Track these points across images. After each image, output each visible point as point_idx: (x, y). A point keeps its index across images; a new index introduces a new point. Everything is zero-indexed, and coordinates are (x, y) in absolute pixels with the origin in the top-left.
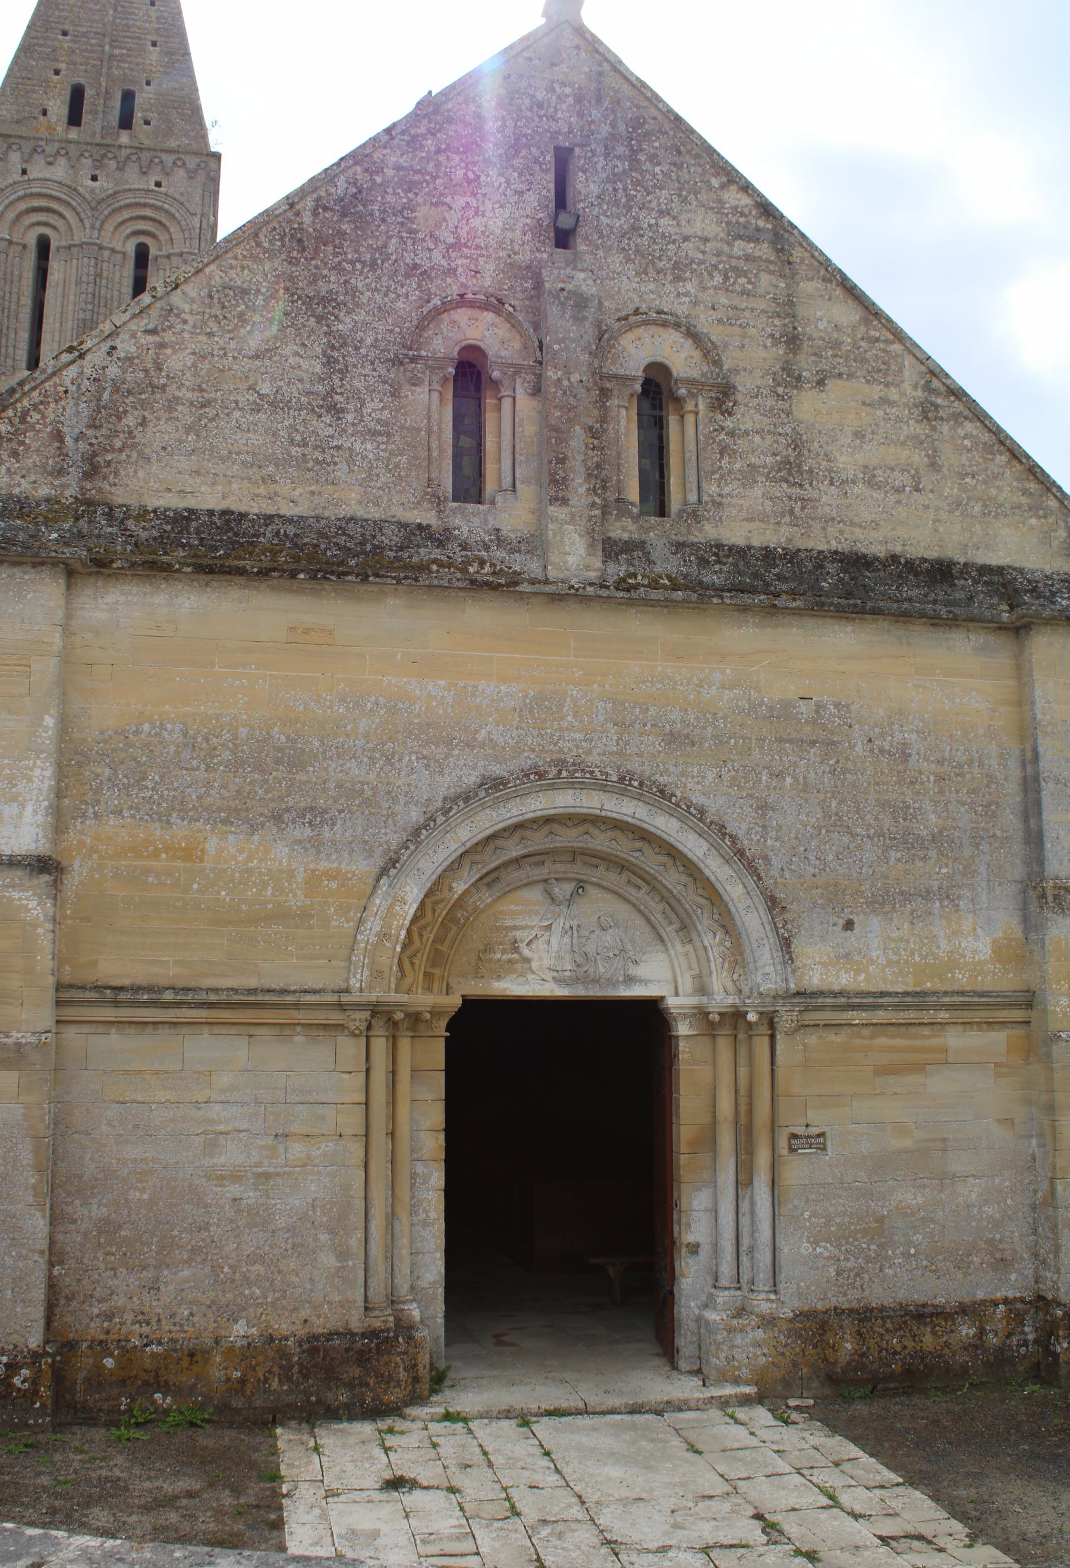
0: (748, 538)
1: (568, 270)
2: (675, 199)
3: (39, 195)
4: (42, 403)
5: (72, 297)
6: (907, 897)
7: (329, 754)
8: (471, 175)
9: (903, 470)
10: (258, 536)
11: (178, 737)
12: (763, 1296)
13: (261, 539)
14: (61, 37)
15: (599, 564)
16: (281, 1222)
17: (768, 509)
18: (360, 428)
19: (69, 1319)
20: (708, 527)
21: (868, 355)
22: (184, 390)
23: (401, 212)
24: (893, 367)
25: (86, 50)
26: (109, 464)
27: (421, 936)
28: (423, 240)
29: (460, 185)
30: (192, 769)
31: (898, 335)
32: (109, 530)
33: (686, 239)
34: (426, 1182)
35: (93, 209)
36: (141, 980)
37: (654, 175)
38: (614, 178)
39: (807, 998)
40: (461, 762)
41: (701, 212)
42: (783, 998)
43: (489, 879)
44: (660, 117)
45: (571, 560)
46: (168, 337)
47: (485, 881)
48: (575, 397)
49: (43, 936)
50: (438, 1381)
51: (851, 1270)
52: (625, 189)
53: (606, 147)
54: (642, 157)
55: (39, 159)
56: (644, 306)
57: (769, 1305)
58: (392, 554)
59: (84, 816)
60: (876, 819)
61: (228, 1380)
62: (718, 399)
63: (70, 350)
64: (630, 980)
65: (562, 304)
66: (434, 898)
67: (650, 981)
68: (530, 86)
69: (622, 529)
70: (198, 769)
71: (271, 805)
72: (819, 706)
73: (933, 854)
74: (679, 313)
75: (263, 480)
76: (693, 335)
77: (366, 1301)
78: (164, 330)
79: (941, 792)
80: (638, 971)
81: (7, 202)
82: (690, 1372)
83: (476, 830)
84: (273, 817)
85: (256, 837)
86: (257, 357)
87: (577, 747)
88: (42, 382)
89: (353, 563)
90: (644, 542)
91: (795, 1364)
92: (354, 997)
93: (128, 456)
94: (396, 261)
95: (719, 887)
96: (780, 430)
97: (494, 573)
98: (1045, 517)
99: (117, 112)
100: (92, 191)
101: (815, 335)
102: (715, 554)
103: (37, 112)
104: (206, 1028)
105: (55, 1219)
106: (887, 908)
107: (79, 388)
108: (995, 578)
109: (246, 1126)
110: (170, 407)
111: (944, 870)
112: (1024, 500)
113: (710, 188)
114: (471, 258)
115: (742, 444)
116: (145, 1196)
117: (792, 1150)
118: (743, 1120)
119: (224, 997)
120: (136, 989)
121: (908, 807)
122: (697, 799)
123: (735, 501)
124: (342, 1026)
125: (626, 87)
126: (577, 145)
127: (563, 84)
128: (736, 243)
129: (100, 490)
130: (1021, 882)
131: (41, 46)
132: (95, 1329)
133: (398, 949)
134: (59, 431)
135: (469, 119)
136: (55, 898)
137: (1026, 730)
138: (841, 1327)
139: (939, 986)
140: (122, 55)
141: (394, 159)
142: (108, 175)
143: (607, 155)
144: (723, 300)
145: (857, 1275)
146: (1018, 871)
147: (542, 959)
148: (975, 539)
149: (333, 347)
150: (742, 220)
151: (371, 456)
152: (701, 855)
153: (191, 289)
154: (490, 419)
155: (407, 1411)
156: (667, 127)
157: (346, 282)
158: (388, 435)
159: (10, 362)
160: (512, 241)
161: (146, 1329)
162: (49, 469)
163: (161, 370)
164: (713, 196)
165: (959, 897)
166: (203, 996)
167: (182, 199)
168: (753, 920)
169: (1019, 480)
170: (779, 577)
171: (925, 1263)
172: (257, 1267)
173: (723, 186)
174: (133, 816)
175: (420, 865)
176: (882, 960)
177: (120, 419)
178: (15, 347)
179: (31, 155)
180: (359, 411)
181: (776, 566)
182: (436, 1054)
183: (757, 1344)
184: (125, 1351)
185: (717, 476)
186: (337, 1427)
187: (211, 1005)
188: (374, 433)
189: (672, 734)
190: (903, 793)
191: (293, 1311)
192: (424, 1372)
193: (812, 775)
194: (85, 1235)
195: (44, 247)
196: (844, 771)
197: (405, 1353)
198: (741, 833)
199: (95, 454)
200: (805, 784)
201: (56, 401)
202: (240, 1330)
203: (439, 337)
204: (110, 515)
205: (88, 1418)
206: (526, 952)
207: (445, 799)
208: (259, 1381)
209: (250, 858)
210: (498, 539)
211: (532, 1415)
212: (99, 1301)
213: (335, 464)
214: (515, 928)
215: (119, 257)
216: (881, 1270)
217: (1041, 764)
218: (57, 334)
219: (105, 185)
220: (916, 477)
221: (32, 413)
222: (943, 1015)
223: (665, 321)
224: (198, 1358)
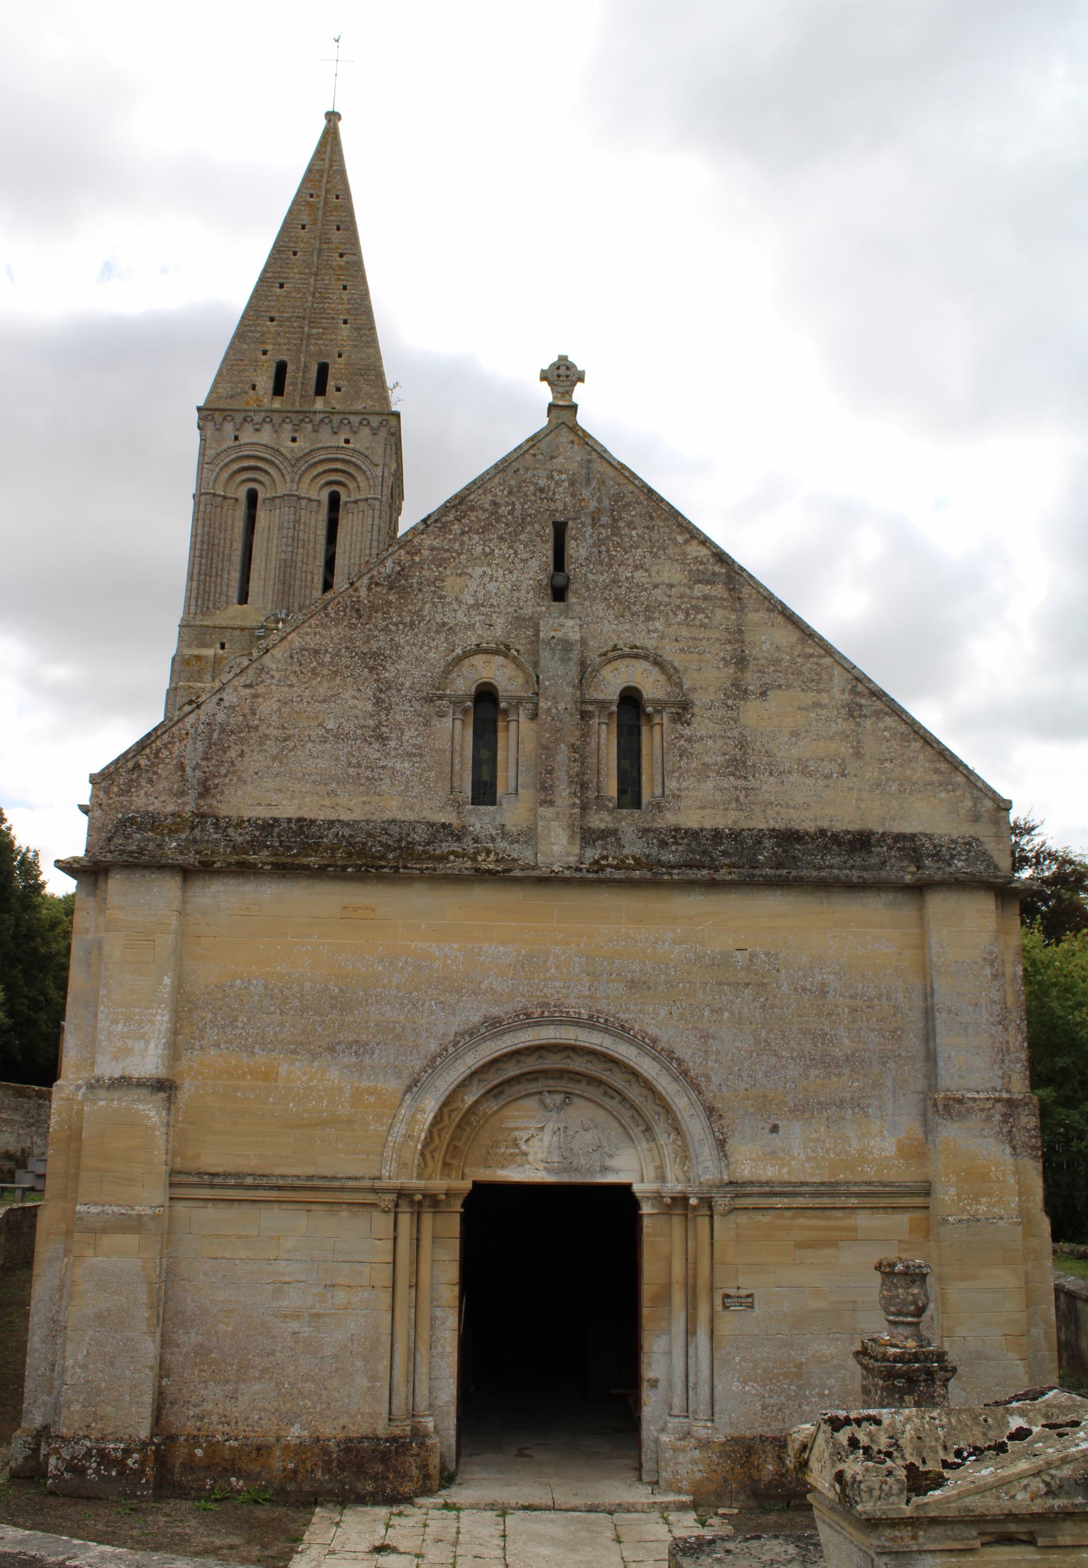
0: (701, 822)
1: (562, 619)
2: (648, 555)
3: (249, 457)
4: (170, 742)
5: (275, 541)
6: (823, 1106)
7: (370, 1001)
8: (487, 550)
9: (831, 760)
10: (322, 838)
12: (702, 1423)
13: (325, 840)
14: (268, 323)
15: (577, 851)
16: (328, 1351)
17: (718, 798)
18: (400, 751)
19: (172, 1418)
21: (803, 669)
22: (271, 729)
23: (434, 583)
24: (824, 677)
25: (289, 332)
26: (217, 786)
27: (440, 1136)
28: (450, 603)
29: (479, 558)
30: (271, 1013)
31: (829, 650)
32: (215, 836)
34: (443, 1323)
35: (292, 466)
36: (231, 1169)
37: (631, 537)
38: (600, 542)
39: (736, 1187)
40: (469, 1006)
41: (668, 564)
42: (717, 1187)
43: (495, 1092)
44: (637, 491)
45: (555, 848)
46: (261, 689)
47: (493, 1093)
48: (561, 721)
50: (448, 1479)
51: (774, 1405)
52: (607, 551)
53: (593, 519)
54: (622, 524)
55: (248, 427)
56: (621, 642)
57: (706, 1431)
58: (420, 848)
59: (193, 1048)
60: (799, 1044)
61: (285, 1469)
62: (678, 713)
64: (605, 1169)
65: (552, 649)
66: (450, 1108)
67: (622, 1170)
68: (534, 476)
69: (599, 820)
70: (274, 1013)
71: (327, 1039)
72: (752, 956)
73: (846, 1071)
74: (649, 646)
75: (328, 794)
76: (658, 663)
77: (390, 1413)
78: (257, 684)
79: (854, 1021)
80: (614, 1163)
81: (222, 464)
82: (649, 1483)
83: (479, 1057)
84: (329, 1048)
85: (316, 1064)
86: (325, 701)
87: (558, 992)
88: (171, 728)
89: (391, 856)
90: (617, 830)
91: (725, 1480)
92: (384, 1183)
93: (231, 780)
95: (668, 1099)
96: (729, 734)
97: (497, 861)
98: (953, 791)
99: (313, 382)
100: (292, 451)
101: (759, 656)
102: (674, 837)
103: (248, 387)
104: (276, 1205)
105: (165, 1343)
106: (807, 1115)
107: (196, 731)
108: (908, 844)
109: (304, 1278)
110: (261, 742)
111: (856, 1084)
112: (936, 778)
113: (676, 543)
114: (486, 615)
115: (697, 747)
116: (230, 1329)
117: (726, 1307)
119: (289, 1182)
120: (227, 1175)
121: (826, 1034)
122: (652, 1031)
123: (691, 793)
124: (375, 1204)
125: (610, 472)
126: (570, 519)
127: (560, 472)
128: (696, 587)
129: (210, 806)
130: (923, 1093)
131: (252, 332)
132: (190, 1427)
133: (419, 1147)
134: (182, 763)
135: (487, 506)
136: (169, 1109)
137: (925, 969)
138: (764, 1452)
139: (850, 1178)
140: (318, 334)
141: (429, 542)
142: (305, 436)
143: (593, 525)
144: (685, 633)
145: (780, 1410)
146: (920, 1084)
147: (537, 1151)
148: (892, 812)
149: (381, 691)
150: (701, 567)
151: (408, 772)
152: (654, 1075)
153: (278, 653)
154: (501, 736)
155: (416, 1500)
156: (642, 498)
157: (391, 640)
158: (421, 755)
159: (224, 598)
160: (518, 599)
161: (227, 1428)
162: (174, 791)
163: (255, 714)
164: (678, 550)
165: (869, 1106)
166: (273, 1182)
167: (367, 453)
168: (695, 1125)
169: (931, 761)
170: (724, 853)
171: (837, 1402)
172: (309, 1384)
173: (686, 542)
174: (228, 1048)
175: (437, 1084)
176: (802, 1157)
177: (225, 752)
178: (228, 585)
179: (242, 424)
180: (399, 739)
181: (722, 844)
182: (453, 1225)
183: (694, 1462)
184: (211, 1444)
185: (677, 774)
186: (360, 1509)
187: (280, 1188)
188: (410, 755)
189: (632, 981)
190: (821, 1023)
191: (334, 1419)
192: (434, 1471)
193: (746, 1009)
194: (186, 1356)
195: (252, 498)
196: (773, 1007)
197: (417, 1455)
198: (687, 1057)
199: (207, 780)
200: (740, 1018)
201: (180, 741)
202: (295, 1433)
203: (461, 678)
204: (216, 825)
205: (181, 1492)
206: (524, 1147)
207: (456, 1034)
208: (307, 1471)
209: (311, 1079)
210: (503, 833)
211: (511, 1508)
212: (194, 1406)
213: (381, 780)
214: (516, 1129)
215: (314, 504)
216: (800, 1406)
217: (936, 998)
218: (263, 572)
219: (303, 444)
220: (842, 766)
222: (853, 1201)
223: (637, 654)
224: (263, 1452)
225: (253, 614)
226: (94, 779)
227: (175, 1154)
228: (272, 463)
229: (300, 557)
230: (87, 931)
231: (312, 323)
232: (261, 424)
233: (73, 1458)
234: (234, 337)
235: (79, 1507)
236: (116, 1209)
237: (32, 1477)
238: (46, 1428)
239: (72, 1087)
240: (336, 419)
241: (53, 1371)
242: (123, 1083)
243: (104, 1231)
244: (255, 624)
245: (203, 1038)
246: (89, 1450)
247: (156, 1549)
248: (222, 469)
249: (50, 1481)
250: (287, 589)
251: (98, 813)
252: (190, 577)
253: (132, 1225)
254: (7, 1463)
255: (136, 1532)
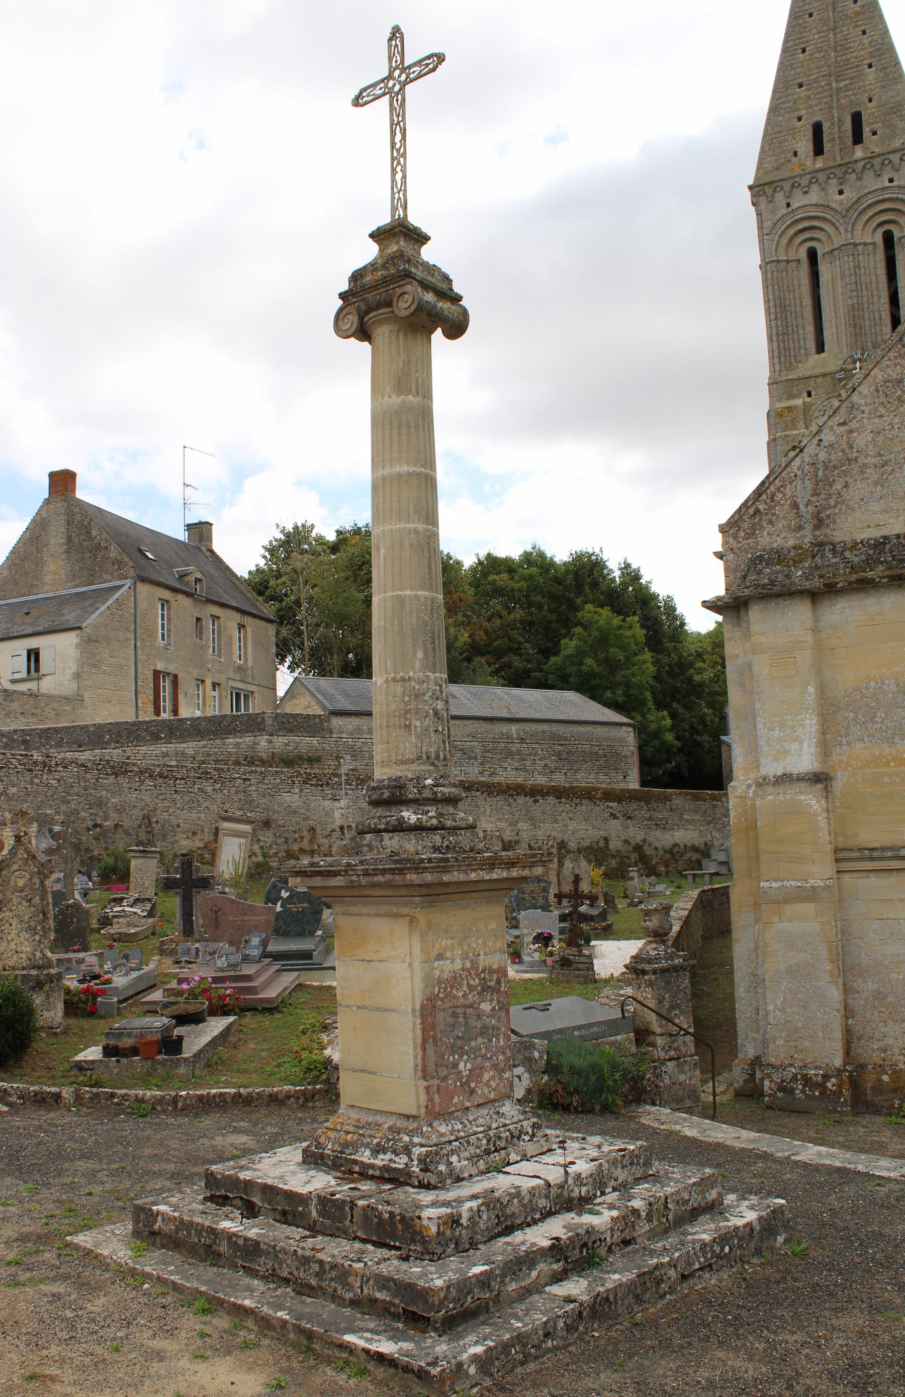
5: (840, 290)
11: (893, 688)
19: (860, 1051)
25: (818, 93)
26: (828, 517)
35: (844, 217)
36: (886, 843)
46: (854, 425)
49: (821, 819)
55: (798, 192)
59: (840, 744)
63: (794, 448)
99: (850, 134)
100: (841, 203)
103: (790, 155)
105: (847, 990)
120: (884, 849)
129: (826, 535)
132: (876, 1057)
136: (827, 797)
142: (850, 187)
153: (864, 389)
159: (803, 352)
177: (831, 486)
178: (804, 339)
179: (791, 191)
184: (895, 1072)
194: (866, 1000)
195: (812, 255)
199: (819, 513)
204: (834, 550)
205: (875, 1110)
215: (870, 248)
225: (831, 360)
226: (723, 529)
227: (837, 835)
228: (824, 219)
229: (865, 299)
230: (737, 656)
231: (839, 77)
232: (808, 186)
233: (783, 1081)
234: (769, 113)
235: (793, 1119)
236: (793, 883)
237: (752, 1096)
238: (758, 1058)
239: (744, 787)
240: (877, 162)
241: (758, 1014)
242: (785, 779)
243: (786, 902)
244: (834, 369)
245: (848, 735)
246: (795, 1075)
247: (862, 1151)
248: (780, 236)
249: (767, 1099)
250: (858, 331)
251: (731, 557)
252: (770, 340)
253: (809, 895)
254: (731, 1085)
255: (841, 1139)
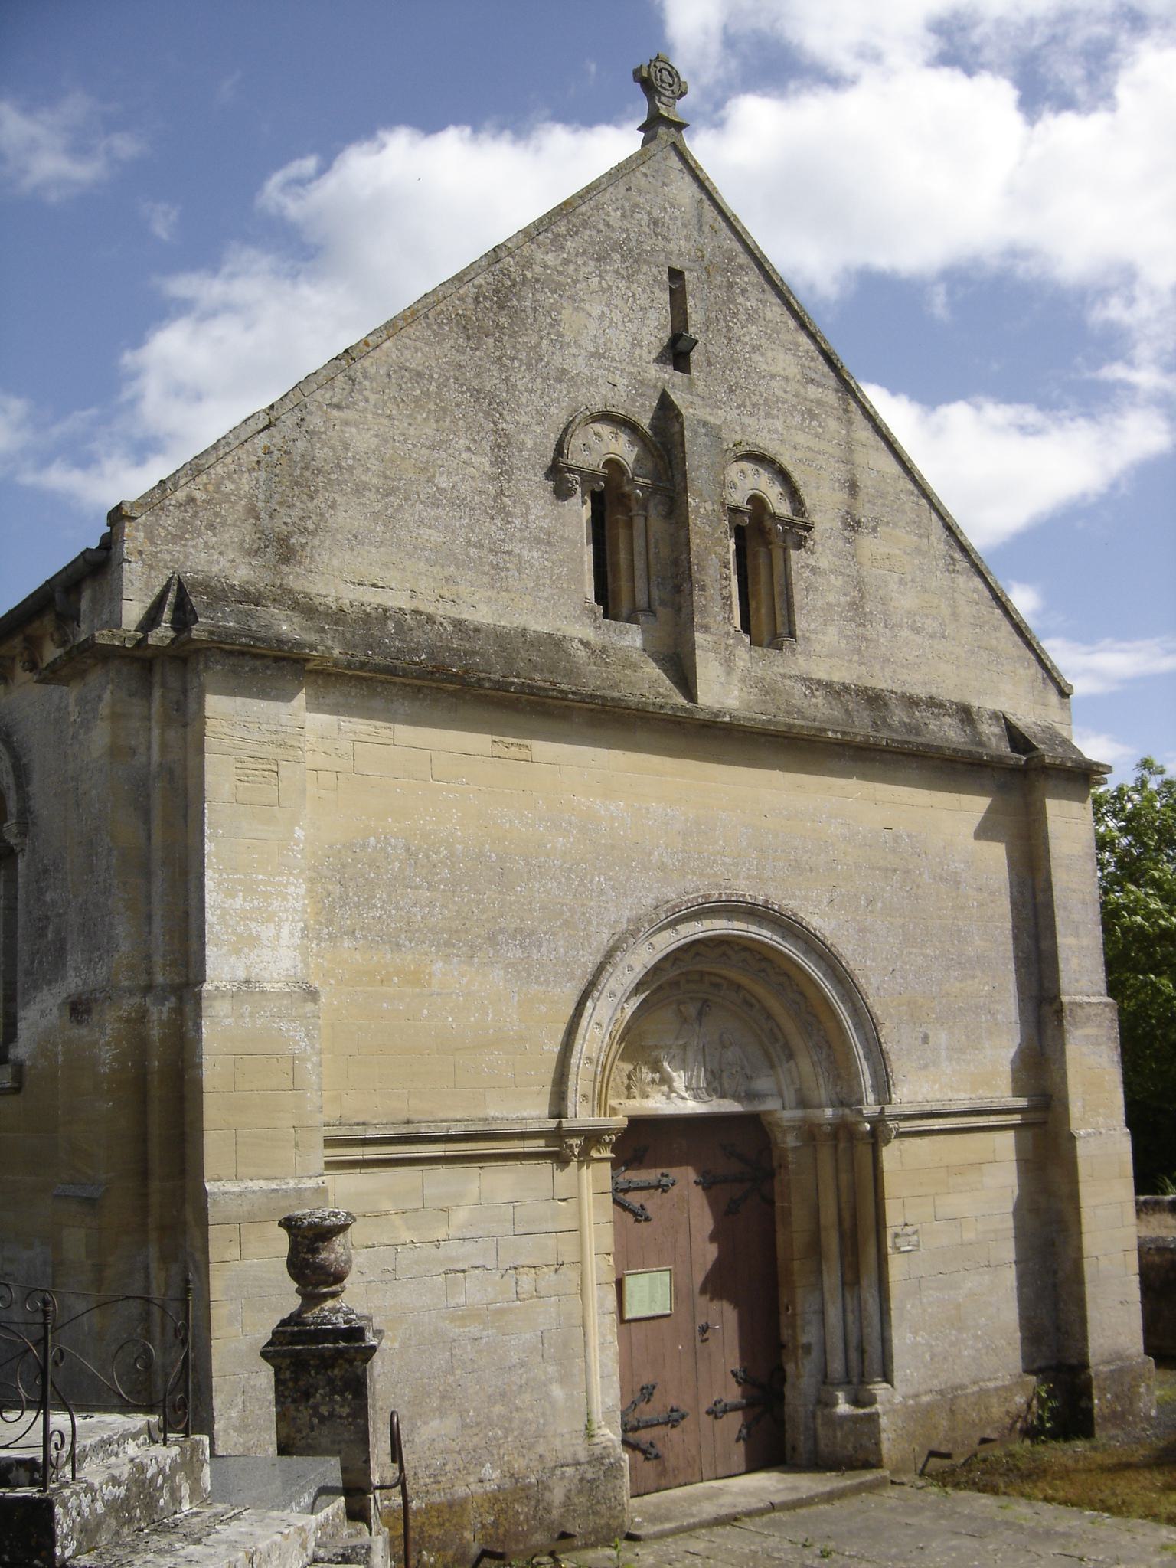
20: (801, 660)
26: (303, 546)
33: (773, 377)
75: (447, 580)
78: (348, 407)
84: (489, 938)
93: (322, 541)
94: (548, 363)
118: (847, 1224)
149: (499, 446)
163: (347, 449)
174: (365, 937)
207: (629, 920)
213: (508, 570)
221: (226, 482)
